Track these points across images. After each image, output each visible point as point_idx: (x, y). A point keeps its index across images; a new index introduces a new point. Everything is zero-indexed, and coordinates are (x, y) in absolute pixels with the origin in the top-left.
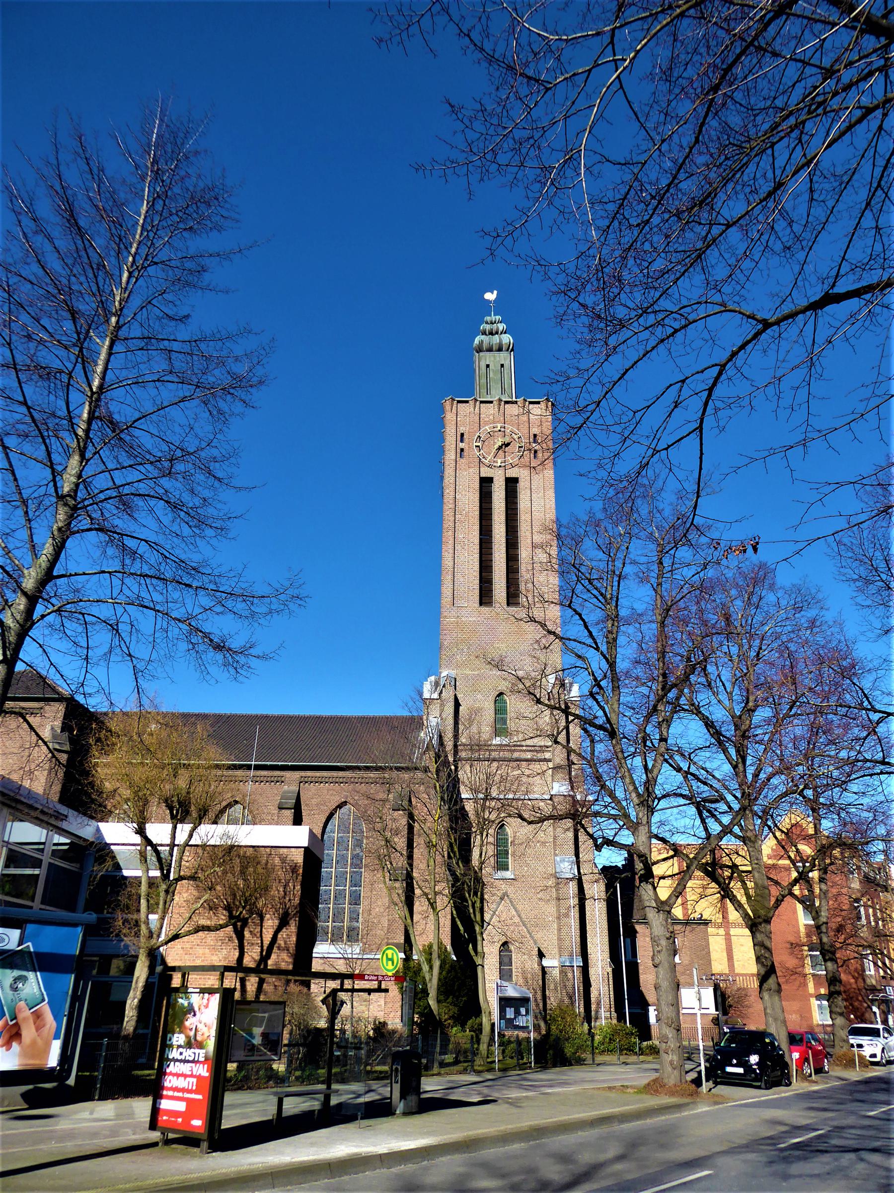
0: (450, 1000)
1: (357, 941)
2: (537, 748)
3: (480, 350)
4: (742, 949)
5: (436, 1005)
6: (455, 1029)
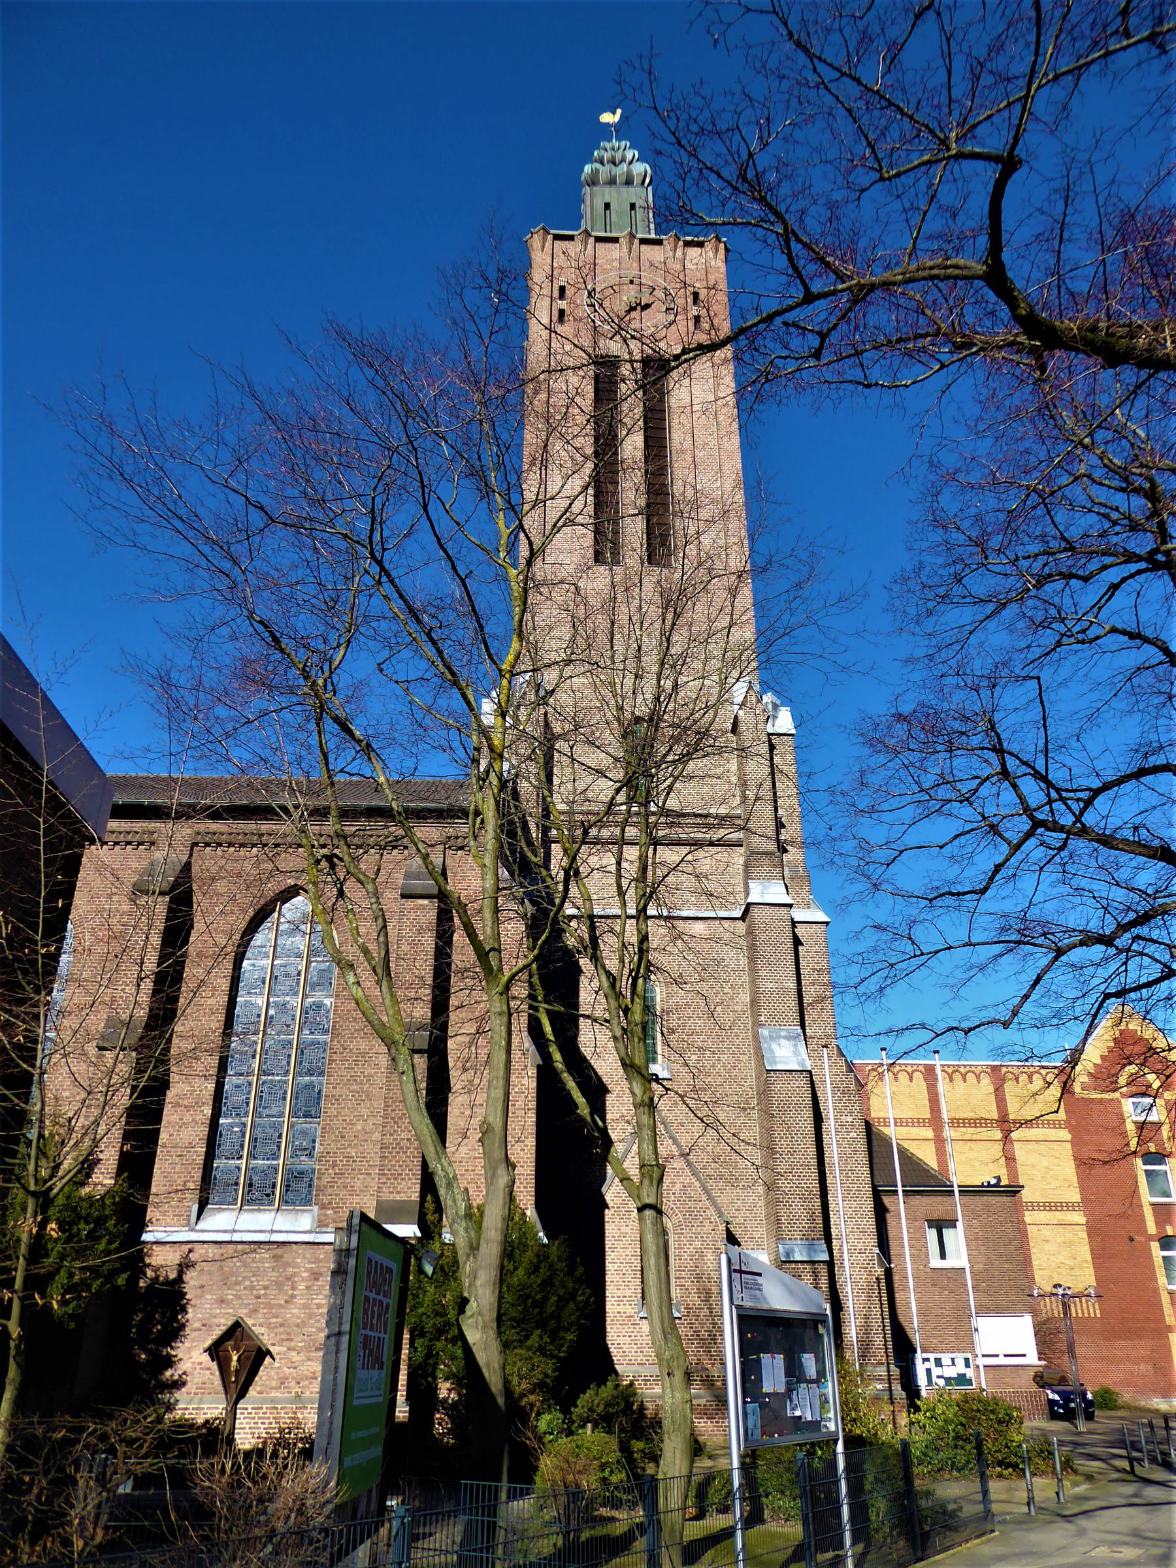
0: (534, 1340)
1: (308, 1202)
2: (711, 821)
3: (593, 181)
4: (1047, 1247)
5: (495, 1345)
6: (546, 1417)
